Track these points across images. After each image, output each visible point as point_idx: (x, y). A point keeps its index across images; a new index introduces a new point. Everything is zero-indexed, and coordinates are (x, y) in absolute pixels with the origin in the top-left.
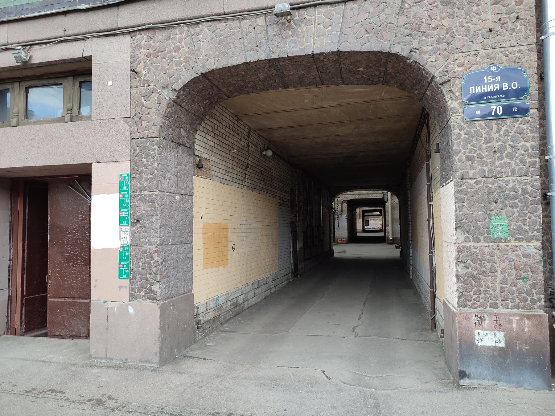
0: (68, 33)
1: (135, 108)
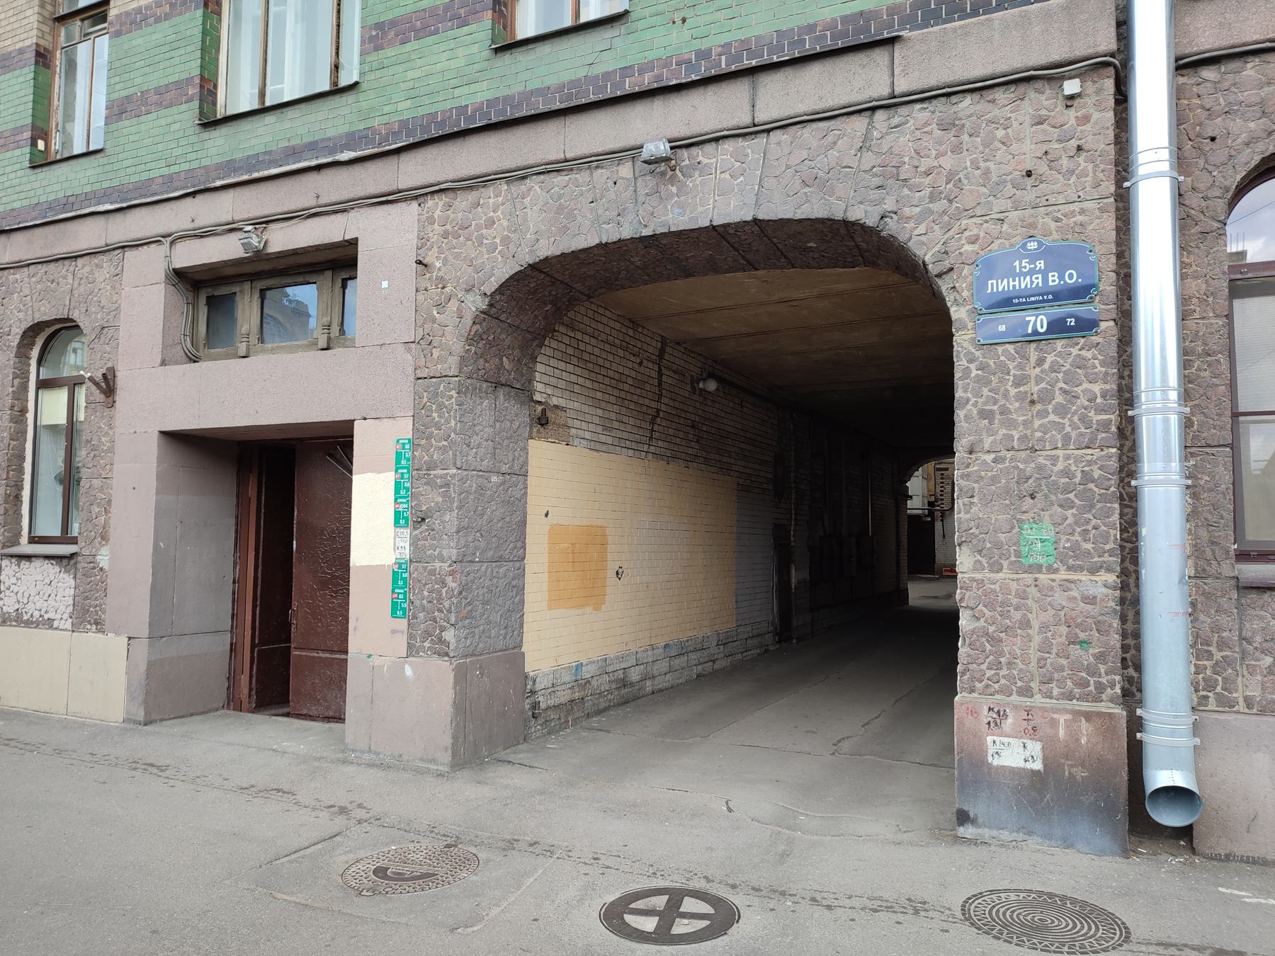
0: (322, 201)
1: (422, 326)
